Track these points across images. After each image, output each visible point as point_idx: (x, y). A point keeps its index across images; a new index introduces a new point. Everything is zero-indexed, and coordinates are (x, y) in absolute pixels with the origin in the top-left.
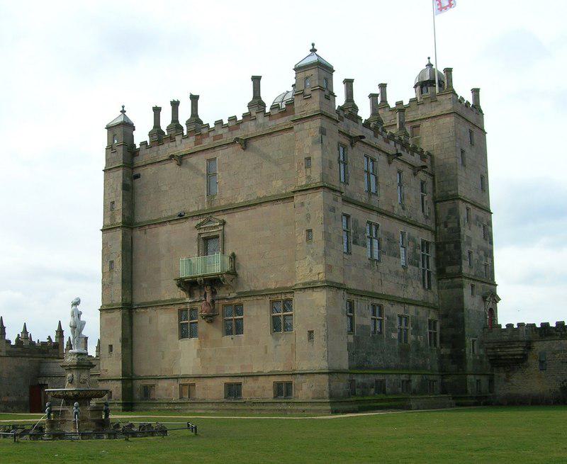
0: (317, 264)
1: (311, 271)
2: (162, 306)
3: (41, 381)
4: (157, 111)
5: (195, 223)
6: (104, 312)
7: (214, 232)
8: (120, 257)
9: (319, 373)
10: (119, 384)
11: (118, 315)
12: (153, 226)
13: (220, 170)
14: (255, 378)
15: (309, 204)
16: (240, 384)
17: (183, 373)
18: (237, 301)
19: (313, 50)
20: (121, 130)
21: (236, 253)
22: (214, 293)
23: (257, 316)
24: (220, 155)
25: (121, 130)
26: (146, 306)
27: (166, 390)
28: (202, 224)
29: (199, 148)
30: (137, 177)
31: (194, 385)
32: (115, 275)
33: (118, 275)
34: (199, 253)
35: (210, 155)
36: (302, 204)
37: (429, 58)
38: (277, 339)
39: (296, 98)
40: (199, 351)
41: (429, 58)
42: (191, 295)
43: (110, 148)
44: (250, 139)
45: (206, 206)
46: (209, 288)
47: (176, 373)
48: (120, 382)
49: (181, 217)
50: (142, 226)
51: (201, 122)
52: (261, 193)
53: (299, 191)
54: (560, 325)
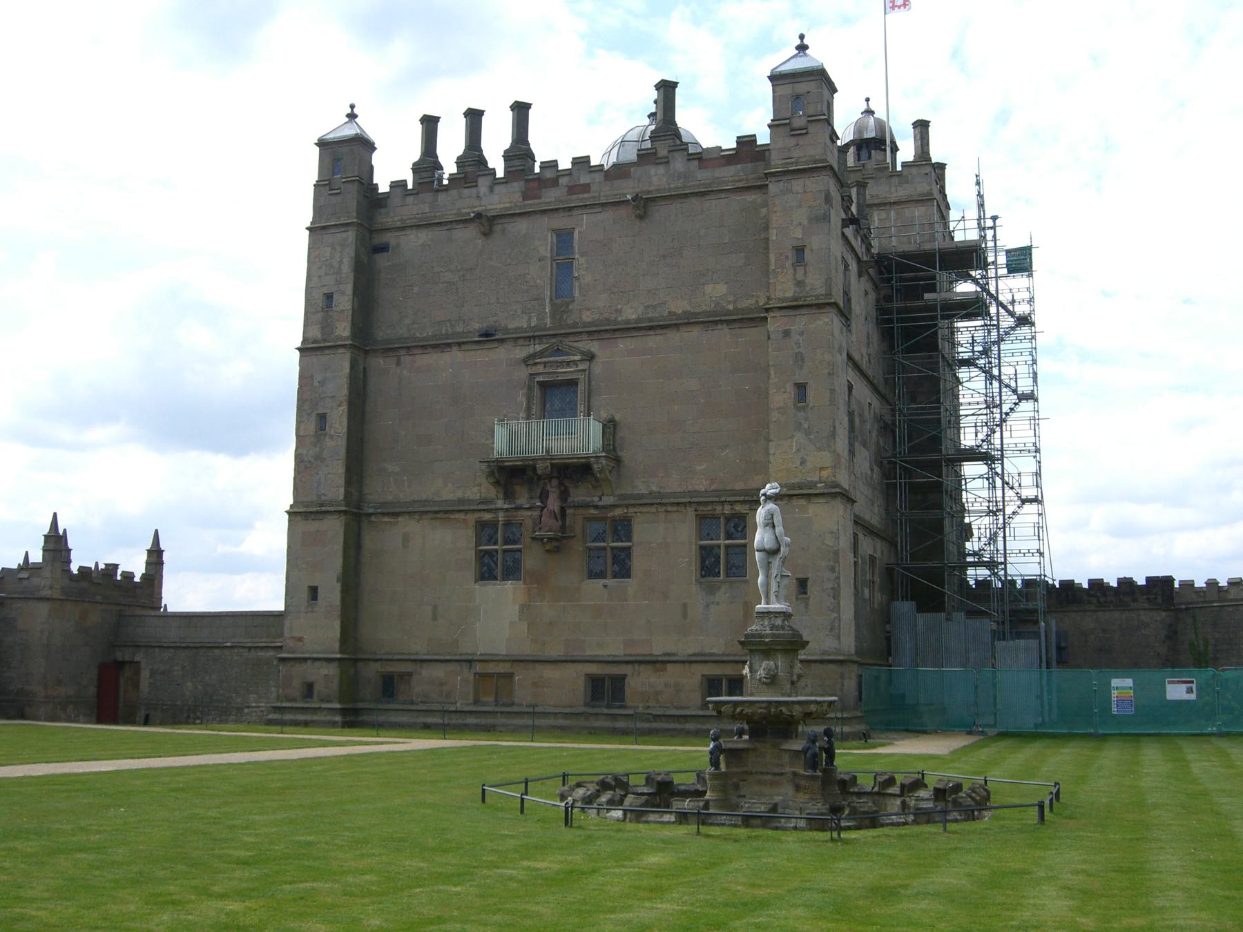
0: (819, 449)
1: (803, 462)
2: (436, 512)
3: (123, 655)
4: (430, 124)
5: (521, 352)
6: (299, 518)
7: (566, 373)
8: (345, 407)
9: (822, 662)
10: (332, 670)
11: (334, 528)
12: (420, 351)
13: (582, 255)
14: (658, 665)
15: (802, 334)
16: (623, 677)
17: (482, 649)
18: (618, 512)
19: (352, 116)
20: (345, 157)
21: (617, 418)
22: (564, 495)
23: (664, 545)
24: (584, 226)
25: (345, 157)
26: (394, 512)
27: (441, 685)
28: (541, 354)
29: (531, 205)
30: (383, 248)
31: (510, 676)
32: (329, 443)
33: (337, 440)
34: (529, 409)
35: (561, 222)
36: (787, 334)
37: (867, 100)
38: (711, 590)
39: (657, 144)
40: (524, 609)
41: (867, 100)
42: (509, 495)
43: (323, 188)
44: (654, 199)
45: (548, 321)
46: (555, 482)
47: (466, 648)
48: (336, 664)
49: (488, 336)
50: (390, 350)
51: (484, 163)
52: (680, 306)
53: (781, 308)
54: (1234, 583)
